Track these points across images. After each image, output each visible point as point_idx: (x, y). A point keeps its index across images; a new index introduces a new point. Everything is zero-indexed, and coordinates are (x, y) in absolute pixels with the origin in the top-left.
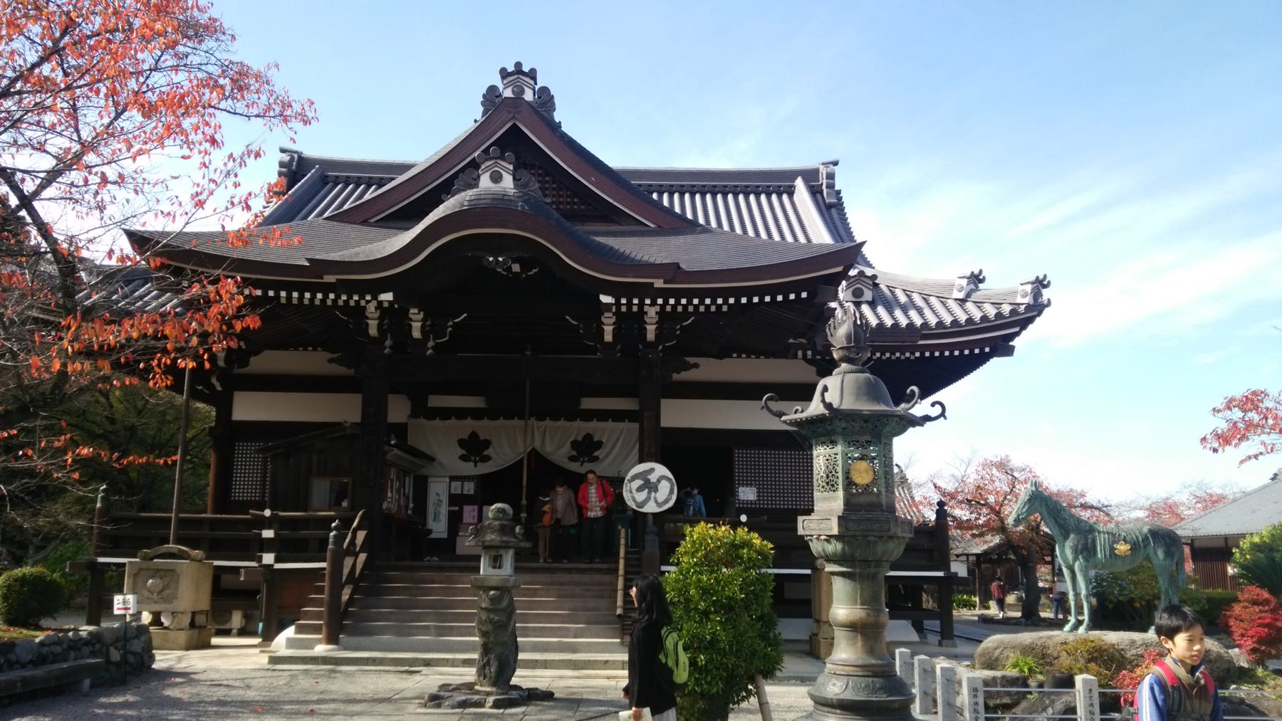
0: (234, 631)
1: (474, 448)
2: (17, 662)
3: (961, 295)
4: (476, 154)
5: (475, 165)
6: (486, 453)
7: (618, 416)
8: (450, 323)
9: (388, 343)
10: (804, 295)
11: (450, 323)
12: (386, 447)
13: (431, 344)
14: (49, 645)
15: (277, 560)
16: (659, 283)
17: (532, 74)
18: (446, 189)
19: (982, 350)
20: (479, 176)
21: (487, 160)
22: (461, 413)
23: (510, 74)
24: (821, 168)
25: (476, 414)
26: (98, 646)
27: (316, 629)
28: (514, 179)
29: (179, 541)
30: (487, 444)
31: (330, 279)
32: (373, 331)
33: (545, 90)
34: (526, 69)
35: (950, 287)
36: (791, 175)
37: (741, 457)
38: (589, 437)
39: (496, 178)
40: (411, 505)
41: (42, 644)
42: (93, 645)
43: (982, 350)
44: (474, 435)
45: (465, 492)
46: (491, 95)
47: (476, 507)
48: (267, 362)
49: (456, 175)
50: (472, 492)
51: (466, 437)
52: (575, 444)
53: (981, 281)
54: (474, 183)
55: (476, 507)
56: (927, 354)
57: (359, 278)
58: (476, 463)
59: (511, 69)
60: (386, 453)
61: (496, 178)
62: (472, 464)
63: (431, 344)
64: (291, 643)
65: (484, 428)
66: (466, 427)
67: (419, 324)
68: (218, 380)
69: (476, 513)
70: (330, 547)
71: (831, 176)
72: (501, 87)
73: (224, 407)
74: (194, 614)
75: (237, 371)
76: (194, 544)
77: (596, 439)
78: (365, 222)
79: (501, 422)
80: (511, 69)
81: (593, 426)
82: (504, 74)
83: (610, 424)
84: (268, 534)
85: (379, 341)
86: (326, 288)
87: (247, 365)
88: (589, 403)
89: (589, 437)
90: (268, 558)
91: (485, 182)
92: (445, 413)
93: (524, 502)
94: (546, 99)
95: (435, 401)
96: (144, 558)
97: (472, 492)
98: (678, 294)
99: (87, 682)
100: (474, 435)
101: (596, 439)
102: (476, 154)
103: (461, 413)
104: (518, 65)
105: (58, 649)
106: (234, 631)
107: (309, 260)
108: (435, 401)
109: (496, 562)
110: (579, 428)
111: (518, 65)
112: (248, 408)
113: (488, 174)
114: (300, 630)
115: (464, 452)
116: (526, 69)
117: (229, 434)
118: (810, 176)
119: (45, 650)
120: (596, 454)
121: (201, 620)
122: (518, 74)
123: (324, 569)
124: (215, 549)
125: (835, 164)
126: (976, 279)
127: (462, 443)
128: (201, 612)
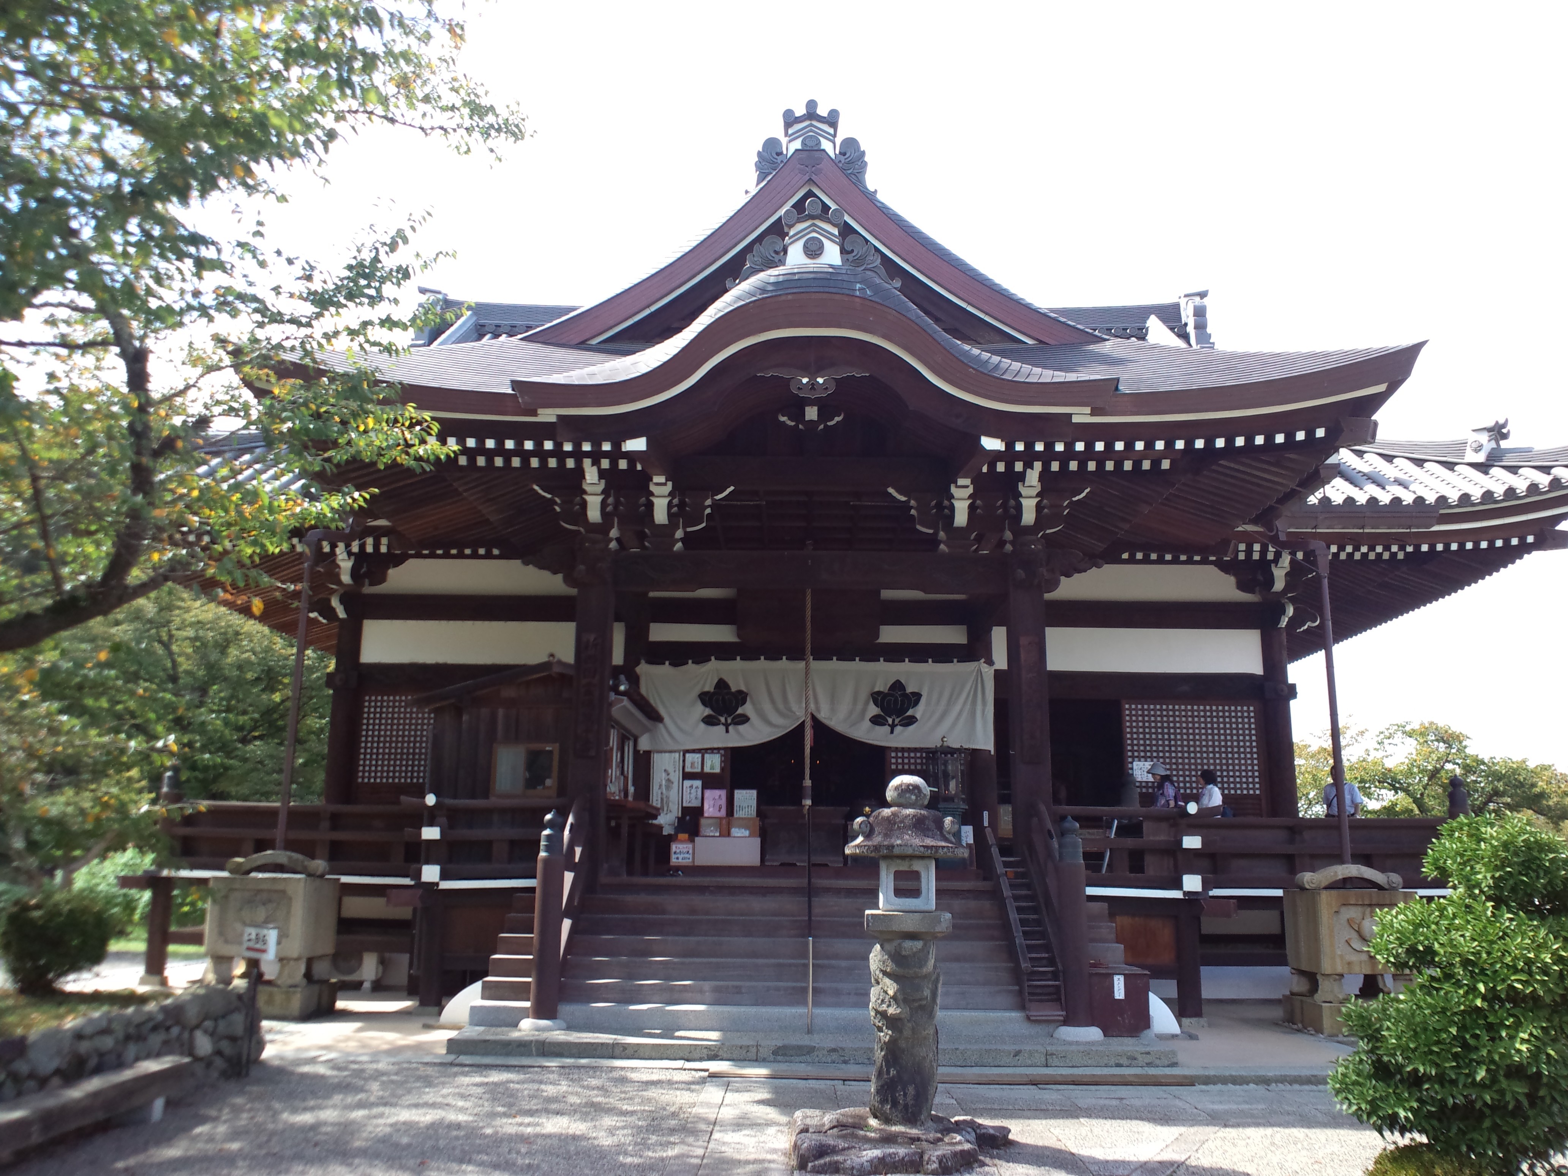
0: (367, 985)
1: (723, 704)
2: (32, 1076)
3: (1481, 458)
4: (782, 212)
5: (778, 230)
6: (740, 711)
7: (941, 653)
8: (708, 502)
9: (614, 533)
10: (1320, 433)
11: (708, 502)
12: (612, 696)
13: (679, 534)
14: (91, 1037)
15: (444, 876)
16: (1081, 415)
17: (832, 120)
18: (734, 271)
19: (1507, 542)
20: (785, 251)
21: (799, 221)
22: (699, 652)
23: (798, 120)
24: (1183, 302)
25: (724, 651)
26: (175, 1031)
27: (518, 992)
28: (843, 251)
29: (290, 845)
30: (741, 697)
31: (547, 415)
32: (594, 514)
33: (851, 144)
34: (822, 111)
35: (1460, 447)
36: (1144, 312)
37: (1134, 716)
38: (898, 686)
39: (813, 250)
40: (631, 789)
41: (78, 1035)
42: (168, 1029)
43: (1507, 542)
44: (722, 684)
45: (707, 769)
46: (770, 158)
47: (723, 793)
48: (414, 575)
49: (749, 248)
50: (717, 770)
51: (709, 687)
52: (877, 698)
53: (1505, 436)
54: (778, 258)
55: (723, 793)
56: (1425, 548)
57: (589, 420)
58: (727, 726)
59: (800, 111)
60: (611, 705)
61: (813, 250)
62: (722, 728)
63: (679, 534)
64: (478, 1016)
65: (736, 672)
66: (706, 674)
67: (665, 501)
68: (342, 602)
69: (723, 802)
70: (543, 854)
71: (1200, 313)
72: (784, 140)
73: (348, 644)
74: (310, 962)
75: (368, 590)
76: (308, 849)
77: (909, 690)
78: (582, 345)
79: (762, 664)
80: (800, 111)
81: (906, 672)
82: (790, 119)
83: (930, 667)
84: (430, 833)
85: (603, 528)
86: (540, 431)
87: (382, 579)
88: (890, 634)
89: (898, 686)
90: (430, 873)
91: (796, 258)
92: (680, 654)
93: (808, 782)
94: (852, 159)
95: (662, 632)
96: (238, 870)
97: (717, 770)
98: (1110, 433)
99: (159, 1104)
100: (722, 684)
101: (909, 690)
102: (782, 212)
103: (699, 652)
104: (812, 105)
105: (108, 1042)
106: (367, 985)
107: (515, 384)
108: (662, 632)
109: (907, 887)
110: (883, 673)
111: (812, 105)
112: (386, 643)
113: (800, 245)
114: (489, 992)
115: (708, 711)
116: (822, 111)
117: (357, 683)
118: (1170, 315)
119: (84, 1047)
120: (910, 713)
121: (321, 969)
122: (812, 119)
123: (532, 890)
124: (341, 856)
125: (1203, 295)
126: (1498, 432)
127: (705, 698)
128: (321, 957)
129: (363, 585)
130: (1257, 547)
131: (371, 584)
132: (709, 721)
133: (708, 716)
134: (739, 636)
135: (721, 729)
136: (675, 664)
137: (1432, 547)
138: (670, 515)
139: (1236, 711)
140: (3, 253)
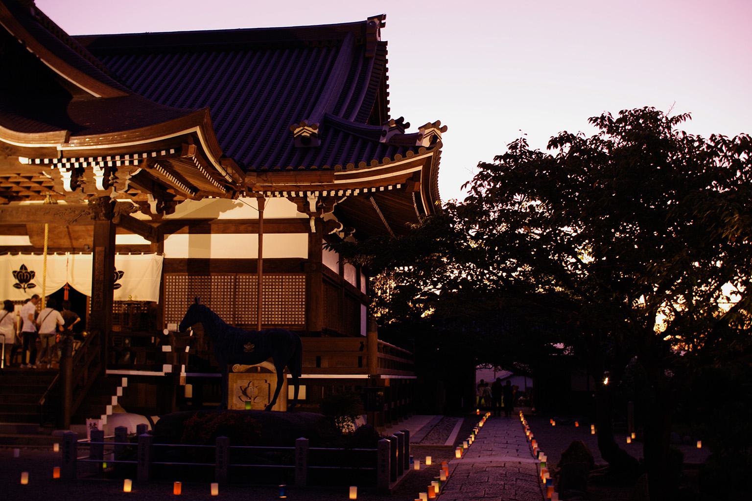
22: (14, 250)
25: (26, 250)
44: (23, 267)
47: (256, 236)
58: (24, 288)
65: (32, 261)
83: (130, 257)
100: (23, 267)
103: (14, 250)
129: (163, 215)
130: (127, 163)
131: (167, 214)
132: (17, 286)
133: (17, 284)
134: (31, 242)
135: (22, 290)
136: (13, 254)
137: (386, 188)
138: (317, 208)
139: (302, 282)
140: (751, 283)
